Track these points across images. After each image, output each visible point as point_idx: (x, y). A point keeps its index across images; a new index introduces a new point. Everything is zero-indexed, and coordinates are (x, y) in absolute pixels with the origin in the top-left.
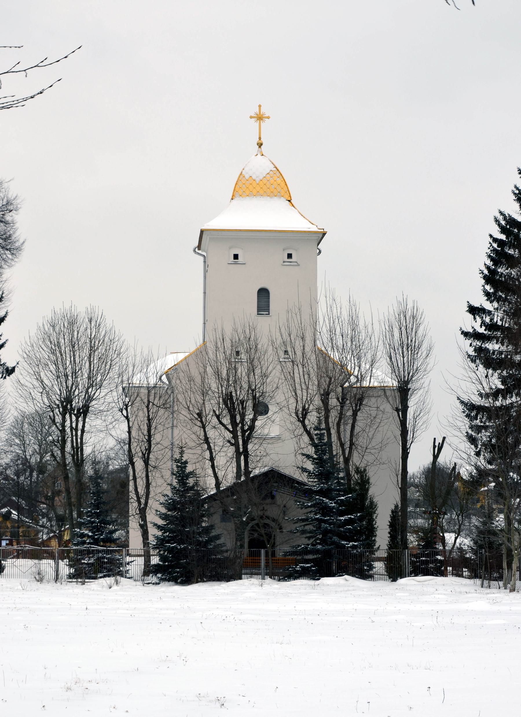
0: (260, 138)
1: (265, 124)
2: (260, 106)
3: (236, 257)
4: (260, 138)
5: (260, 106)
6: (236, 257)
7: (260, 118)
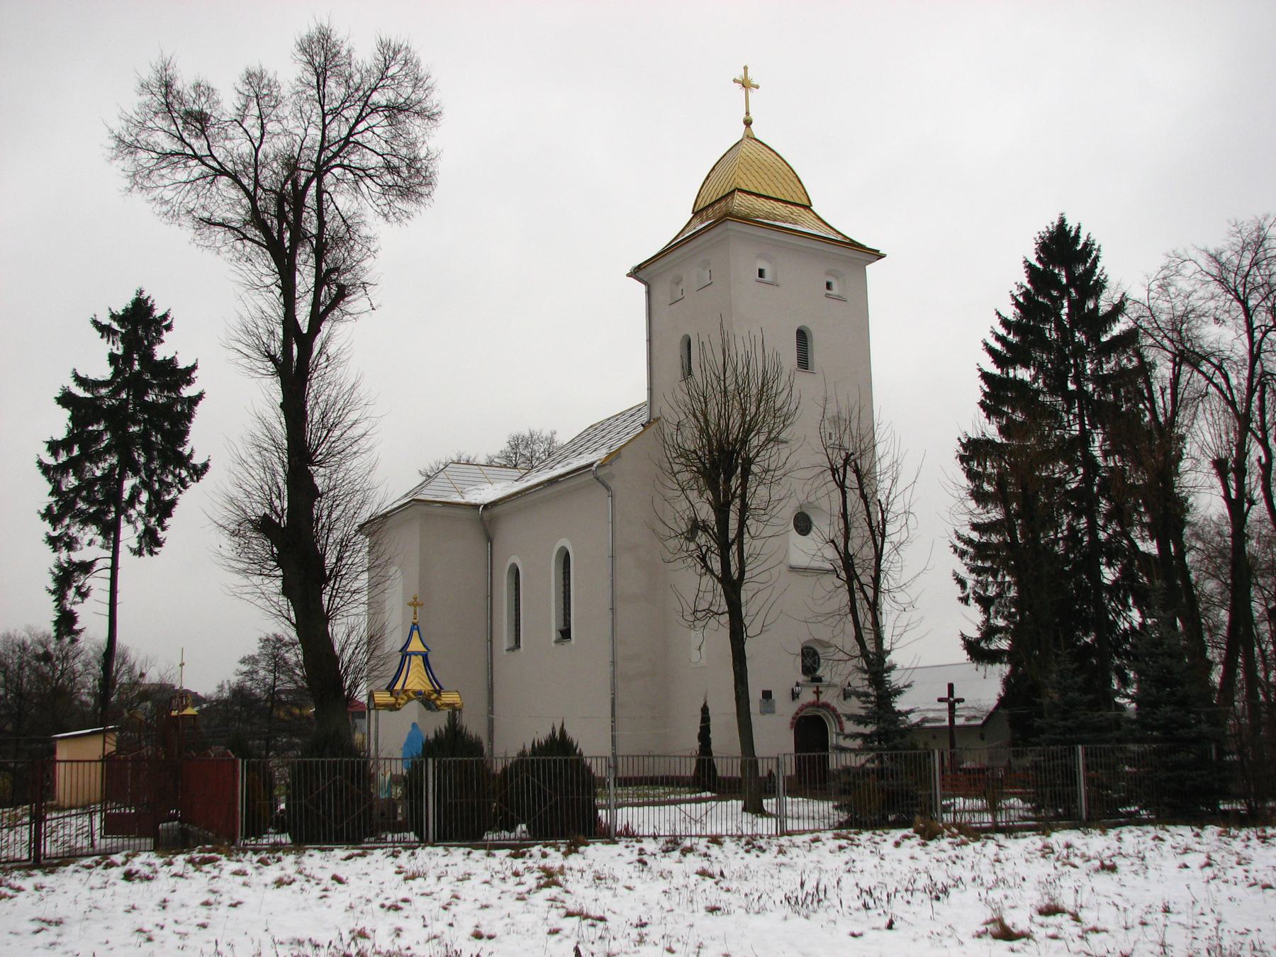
0: (747, 113)
1: (753, 94)
2: (746, 68)
3: (761, 273)
4: (747, 113)
5: (746, 68)
6: (761, 273)
7: (746, 84)
